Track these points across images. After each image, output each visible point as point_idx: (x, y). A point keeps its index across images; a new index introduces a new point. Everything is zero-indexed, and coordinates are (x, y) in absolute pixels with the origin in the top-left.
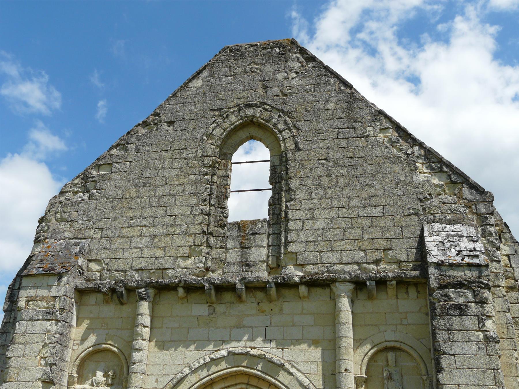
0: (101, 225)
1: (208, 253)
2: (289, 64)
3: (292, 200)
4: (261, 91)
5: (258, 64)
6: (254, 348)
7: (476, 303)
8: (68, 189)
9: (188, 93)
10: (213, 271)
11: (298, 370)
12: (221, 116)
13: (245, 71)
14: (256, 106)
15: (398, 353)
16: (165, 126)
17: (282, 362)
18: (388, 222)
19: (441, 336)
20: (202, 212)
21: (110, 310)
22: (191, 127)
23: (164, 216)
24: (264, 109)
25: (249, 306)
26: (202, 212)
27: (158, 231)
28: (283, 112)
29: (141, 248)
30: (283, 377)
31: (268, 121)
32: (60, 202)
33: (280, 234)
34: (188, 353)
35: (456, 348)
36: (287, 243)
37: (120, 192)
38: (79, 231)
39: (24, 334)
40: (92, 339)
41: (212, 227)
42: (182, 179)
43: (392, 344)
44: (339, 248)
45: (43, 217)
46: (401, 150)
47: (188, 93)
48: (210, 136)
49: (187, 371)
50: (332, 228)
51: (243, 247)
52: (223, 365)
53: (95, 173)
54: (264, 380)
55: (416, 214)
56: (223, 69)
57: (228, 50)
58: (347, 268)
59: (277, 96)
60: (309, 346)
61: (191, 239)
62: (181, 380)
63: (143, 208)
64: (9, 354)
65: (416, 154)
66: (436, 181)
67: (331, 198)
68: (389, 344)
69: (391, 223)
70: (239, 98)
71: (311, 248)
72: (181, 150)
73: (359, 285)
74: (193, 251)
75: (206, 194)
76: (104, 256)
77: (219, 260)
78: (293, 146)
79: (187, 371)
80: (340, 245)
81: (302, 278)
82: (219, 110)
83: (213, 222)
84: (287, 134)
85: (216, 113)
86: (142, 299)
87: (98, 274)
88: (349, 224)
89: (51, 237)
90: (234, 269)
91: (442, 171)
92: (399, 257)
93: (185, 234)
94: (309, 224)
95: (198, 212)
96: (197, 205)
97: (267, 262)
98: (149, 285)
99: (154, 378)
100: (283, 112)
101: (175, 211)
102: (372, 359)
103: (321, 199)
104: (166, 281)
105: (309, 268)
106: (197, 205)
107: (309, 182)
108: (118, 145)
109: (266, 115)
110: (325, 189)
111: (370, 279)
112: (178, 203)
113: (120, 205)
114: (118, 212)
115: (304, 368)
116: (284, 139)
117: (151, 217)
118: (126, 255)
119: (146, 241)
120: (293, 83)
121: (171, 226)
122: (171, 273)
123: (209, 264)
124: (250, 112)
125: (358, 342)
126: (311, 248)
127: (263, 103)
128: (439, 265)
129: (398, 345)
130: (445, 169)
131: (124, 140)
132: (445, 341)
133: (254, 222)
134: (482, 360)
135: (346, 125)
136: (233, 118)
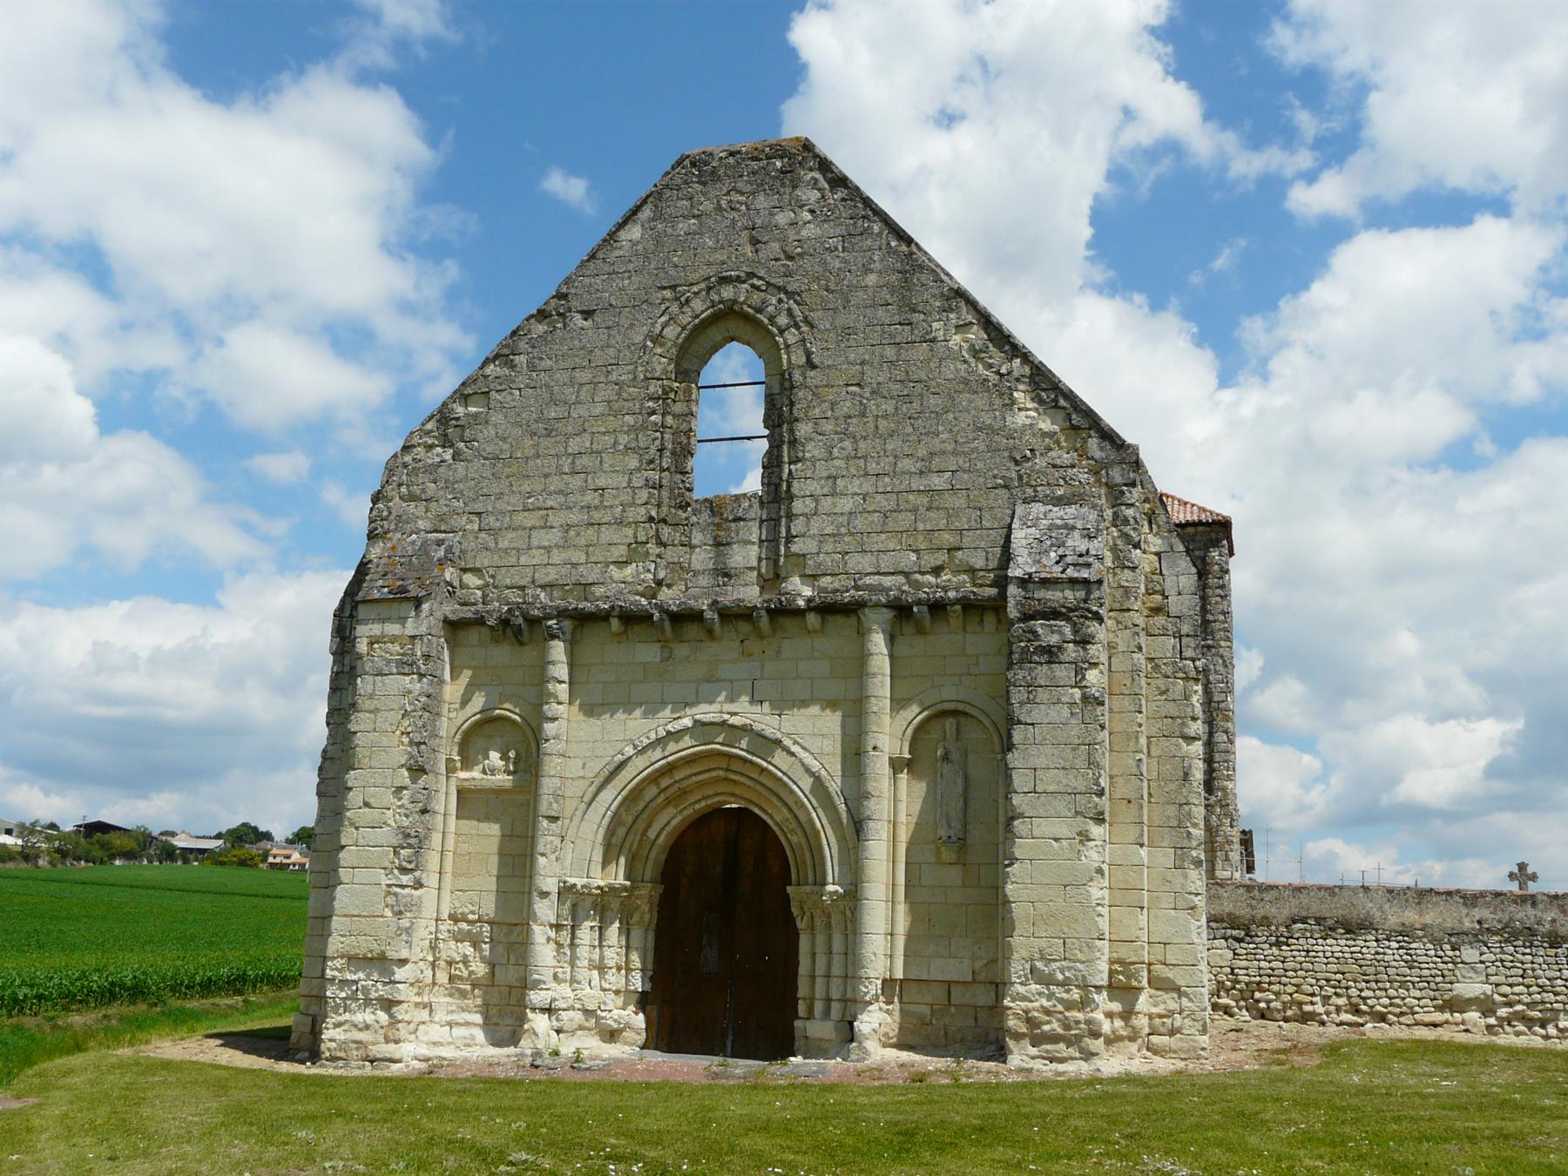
0: (478, 507)
1: (659, 556)
5: (742, 194)
6: (736, 714)
7: (1075, 642)
8: (416, 440)
9: (617, 253)
10: (669, 586)
11: (804, 748)
13: (719, 208)
14: (738, 279)
15: (962, 719)
16: (578, 320)
17: (779, 735)
18: (960, 502)
19: (1017, 696)
21: (502, 654)
24: (753, 286)
25: (726, 648)
27: (574, 517)
28: (786, 293)
30: (780, 758)
31: (760, 311)
32: (405, 466)
33: (778, 520)
34: (630, 724)
35: (1038, 714)
36: (790, 538)
37: (506, 447)
38: (442, 518)
39: (371, 696)
40: (478, 701)
41: (665, 509)
42: (612, 423)
43: (951, 706)
44: (876, 547)
45: (379, 492)
46: (991, 366)
48: (658, 339)
49: (630, 751)
50: (865, 511)
51: (718, 544)
52: (687, 741)
53: (460, 410)
54: (751, 762)
55: (1006, 487)
56: (680, 204)
57: (687, 162)
58: (887, 581)
59: (777, 260)
60: (823, 709)
62: (622, 765)
63: (546, 476)
64: (352, 727)
65: (1016, 374)
66: (1046, 425)
67: (865, 457)
68: (947, 706)
70: (709, 264)
71: (829, 547)
73: (901, 611)
74: (635, 553)
75: (653, 450)
76: (486, 563)
77: (678, 567)
79: (630, 751)
80: (879, 542)
81: (809, 600)
82: (673, 288)
84: (792, 336)
85: (668, 294)
86: (553, 637)
87: (479, 593)
88: (893, 505)
90: (704, 581)
91: (1057, 407)
92: (972, 561)
93: (620, 523)
94: (826, 503)
95: (640, 483)
96: (638, 470)
97: (759, 569)
98: (562, 614)
99: (580, 763)
101: (601, 483)
105: (825, 581)
106: (638, 470)
107: (828, 427)
108: (497, 357)
109: (756, 298)
111: (919, 602)
112: (606, 466)
116: (787, 346)
117: (561, 492)
118: (523, 560)
119: (554, 536)
120: (804, 233)
121: (596, 508)
124: (727, 292)
125: (898, 703)
127: (751, 275)
128: (1024, 582)
129: (960, 707)
130: (1062, 402)
132: (1021, 704)
134: (1074, 731)
135: (897, 319)
136: (698, 305)
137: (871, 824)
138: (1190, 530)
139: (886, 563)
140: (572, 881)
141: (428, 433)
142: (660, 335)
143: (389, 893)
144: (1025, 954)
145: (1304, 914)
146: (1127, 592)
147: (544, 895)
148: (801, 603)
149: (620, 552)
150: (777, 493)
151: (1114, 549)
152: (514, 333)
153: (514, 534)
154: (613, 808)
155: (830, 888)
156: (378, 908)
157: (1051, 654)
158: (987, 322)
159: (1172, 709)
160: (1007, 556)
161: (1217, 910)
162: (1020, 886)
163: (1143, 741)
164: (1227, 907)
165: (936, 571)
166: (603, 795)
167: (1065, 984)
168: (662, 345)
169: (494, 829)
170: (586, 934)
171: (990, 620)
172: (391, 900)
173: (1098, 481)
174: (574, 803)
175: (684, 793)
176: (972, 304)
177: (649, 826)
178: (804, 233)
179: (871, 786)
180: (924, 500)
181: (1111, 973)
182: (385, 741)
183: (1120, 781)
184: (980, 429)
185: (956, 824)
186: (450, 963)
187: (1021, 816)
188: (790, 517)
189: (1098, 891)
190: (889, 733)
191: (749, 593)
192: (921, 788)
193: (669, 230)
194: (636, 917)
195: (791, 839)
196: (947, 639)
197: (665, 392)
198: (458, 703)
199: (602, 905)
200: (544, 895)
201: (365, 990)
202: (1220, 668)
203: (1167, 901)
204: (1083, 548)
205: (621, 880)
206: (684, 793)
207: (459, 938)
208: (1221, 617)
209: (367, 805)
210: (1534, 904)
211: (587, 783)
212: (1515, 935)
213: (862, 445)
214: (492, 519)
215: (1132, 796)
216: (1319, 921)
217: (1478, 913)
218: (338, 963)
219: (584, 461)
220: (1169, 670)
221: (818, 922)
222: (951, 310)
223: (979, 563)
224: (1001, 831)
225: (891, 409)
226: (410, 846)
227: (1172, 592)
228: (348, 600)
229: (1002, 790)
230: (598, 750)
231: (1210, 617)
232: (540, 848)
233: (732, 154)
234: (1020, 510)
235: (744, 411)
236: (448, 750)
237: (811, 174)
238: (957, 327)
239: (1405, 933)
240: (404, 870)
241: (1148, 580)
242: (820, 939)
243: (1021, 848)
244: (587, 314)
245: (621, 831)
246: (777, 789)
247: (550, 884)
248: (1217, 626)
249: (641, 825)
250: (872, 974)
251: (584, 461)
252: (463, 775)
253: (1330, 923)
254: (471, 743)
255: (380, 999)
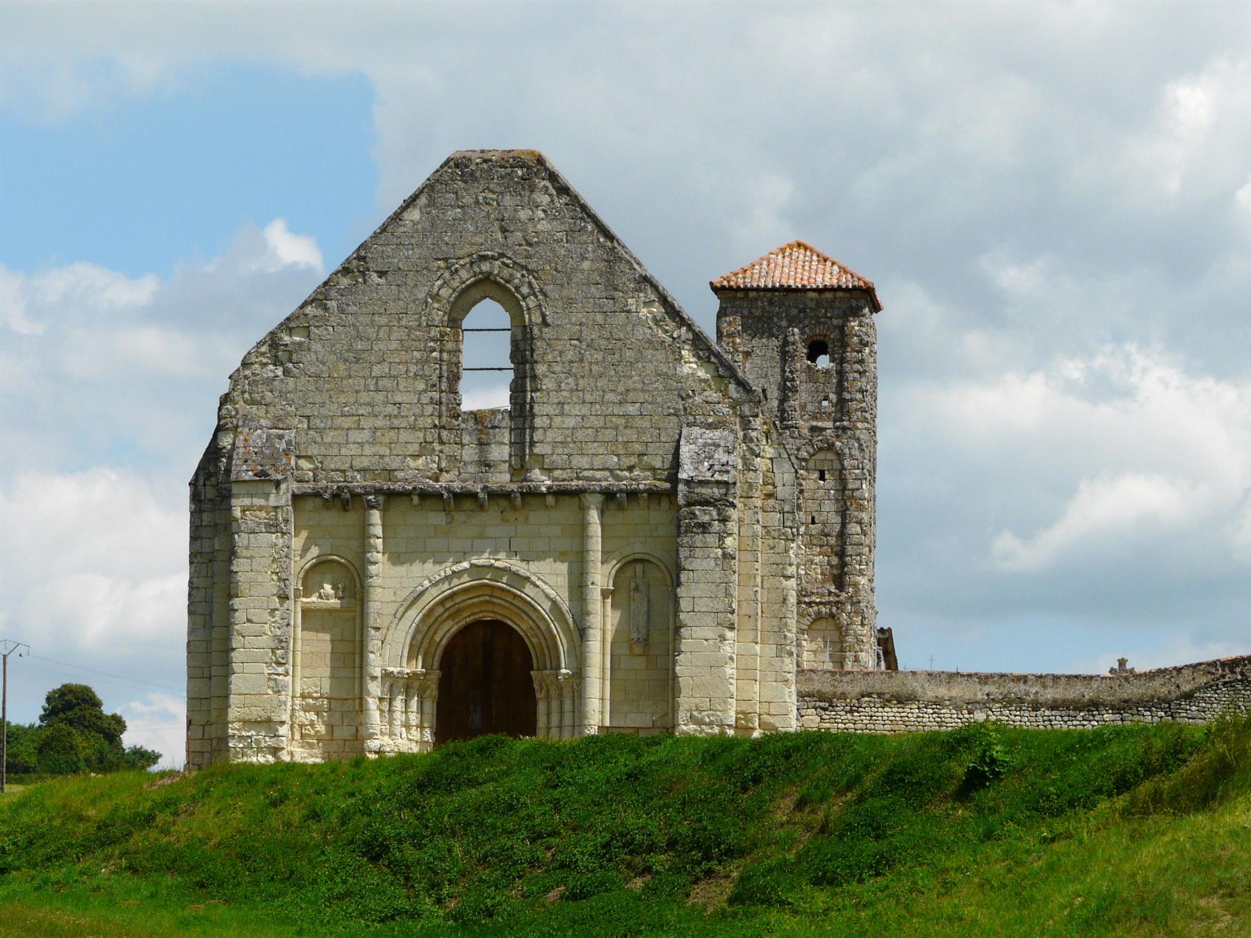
0: (307, 412)
1: (441, 451)
2: (534, 196)
3: (536, 390)
4: (499, 235)
5: (494, 193)
7: (719, 521)
8: (253, 359)
9: (402, 229)
10: (447, 472)
12: (448, 268)
13: (477, 202)
14: (493, 258)
15: (646, 565)
16: (374, 276)
18: (645, 423)
19: (683, 553)
20: (432, 401)
21: (332, 518)
22: (411, 283)
23: (386, 403)
24: (503, 263)
25: (491, 516)
26: (432, 401)
27: (379, 423)
28: (527, 270)
29: (359, 446)
30: (529, 589)
31: (508, 281)
32: (246, 377)
33: (525, 429)
35: (695, 564)
36: (532, 443)
37: (325, 368)
38: (279, 419)
39: (247, 548)
40: (314, 551)
41: (444, 419)
42: (404, 356)
43: (640, 556)
44: (590, 452)
45: (227, 395)
46: (667, 332)
47: (402, 229)
48: (436, 297)
49: (427, 583)
50: (583, 427)
51: (481, 444)
52: (466, 578)
53: (287, 339)
54: (509, 591)
55: (675, 415)
56: (448, 196)
57: (452, 163)
58: (598, 474)
59: (520, 245)
61: (421, 435)
62: (422, 594)
63: (357, 392)
64: (234, 568)
65: (683, 338)
66: (701, 374)
67: (583, 390)
68: (637, 556)
69: (648, 424)
70: (471, 244)
71: (559, 450)
72: (399, 316)
73: (609, 495)
74: (425, 449)
75: (435, 378)
76: (315, 452)
77: (452, 459)
78: (539, 320)
79: (427, 583)
80: (592, 448)
81: (549, 488)
82: (446, 260)
83: (445, 414)
84: (532, 302)
85: (441, 264)
86: (373, 507)
87: (311, 474)
88: (602, 424)
89: (243, 426)
90: (472, 469)
91: (709, 361)
92: (654, 463)
93: (413, 428)
94: (557, 420)
95: (427, 401)
96: (425, 391)
97: (510, 462)
98: (377, 492)
99: (392, 592)
100: (527, 270)
101: (398, 399)
102: (618, 571)
103: (571, 391)
104: (398, 486)
105: (557, 473)
106: (425, 391)
107: (558, 368)
108: (313, 301)
109: (506, 273)
110: (577, 379)
111: (621, 491)
112: (401, 387)
113: (327, 386)
114: (325, 396)
115: (551, 580)
116: (529, 309)
117: (369, 404)
118: (343, 451)
119: (364, 436)
120: (539, 227)
121: (396, 416)
122: (400, 475)
123: (443, 464)
124: (485, 267)
125: (606, 556)
126: (559, 450)
127: (502, 255)
128: (688, 482)
130: (713, 359)
131: (321, 293)
132: (686, 558)
133: (494, 412)
134: (718, 574)
135: (604, 295)
136: (464, 274)
137: (591, 631)
138: (829, 295)
139: (597, 462)
140: (390, 669)
141: (263, 354)
142: (437, 294)
143: (270, 679)
144: (686, 707)
145: (870, 690)
146: (751, 486)
147: (374, 678)
148: (544, 489)
149: (414, 448)
150: (521, 412)
151: (744, 458)
152: (326, 283)
153: (335, 433)
154: (417, 621)
155: (564, 671)
156: (264, 689)
157: (705, 528)
158: (664, 301)
159: (777, 559)
160: (676, 464)
161: (805, 688)
162: (684, 667)
163: (759, 579)
164: (817, 686)
165: (631, 469)
166: (409, 613)
167: (710, 724)
168: (438, 301)
169: (327, 637)
170: (398, 704)
171: (665, 503)
172: (272, 684)
173: (735, 413)
174: (391, 618)
175: (459, 611)
176: (655, 287)
177: (435, 633)
178: (539, 227)
179: (591, 607)
180: (622, 421)
181: (737, 719)
182: (260, 578)
183: (744, 604)
184: (660, 375)
185: (643, 631)
186: (301, 726)
187: (685, 626)
188: (533, 429)
189: (730, 670)
190: (600, 576)
191: (501, 479)
192: (618, 614)
193: (441, 216)
194: (428, 692)
195: (532, 642)
196: (636, 514)
197: (442, 336)
198: (300, 550)
199: (408, 685)
200: (374, 678)
201: (258, 741)
202: (856, 452)
203: (771, 676)
204: (724, 460)
205: (419, 669)
206: (459, 611)
207: (306, 709)
208: (859, 396)
209: (249, 621)
210: (1025, 682)
211: (397, 605)
212: (1010, 703)
213: (581, 382)
214: (318, 421)
215: (751, 613)
216: (880, 695)
217: (987, 689)
218: (236, 725)
219: (383, 383)
220: (776, 534)
221: (553, 692)
222: (641, 291)
223: (658, 464)
224: (671, 635)
225: (600, 358)
226: (283, 648)
227: (779, 484)
228: (201, 473)
229: (671, 610)
230: (405, 590)
231: (847, 396)
232: (370, 648)
233: (485, 161)
234: (685, 431)
235: (499, 349)
236: (295, 584)
237: (544, 183)
238: (644, 303)
239: (938, 703)
240: (279, 664)
241: (765, 476)
242: (555, 704)
243: (685, 644)
244: (382, 274)
245: (419, 637)
246: (527, 608)
247: (377, 672)
248: (853, 405)
249: (432, 631)
250: (592, 722)
251: (383, 383)
252: (304, 600)
253: (887, 696)
254: (310, 580)
255: (269, 747)
